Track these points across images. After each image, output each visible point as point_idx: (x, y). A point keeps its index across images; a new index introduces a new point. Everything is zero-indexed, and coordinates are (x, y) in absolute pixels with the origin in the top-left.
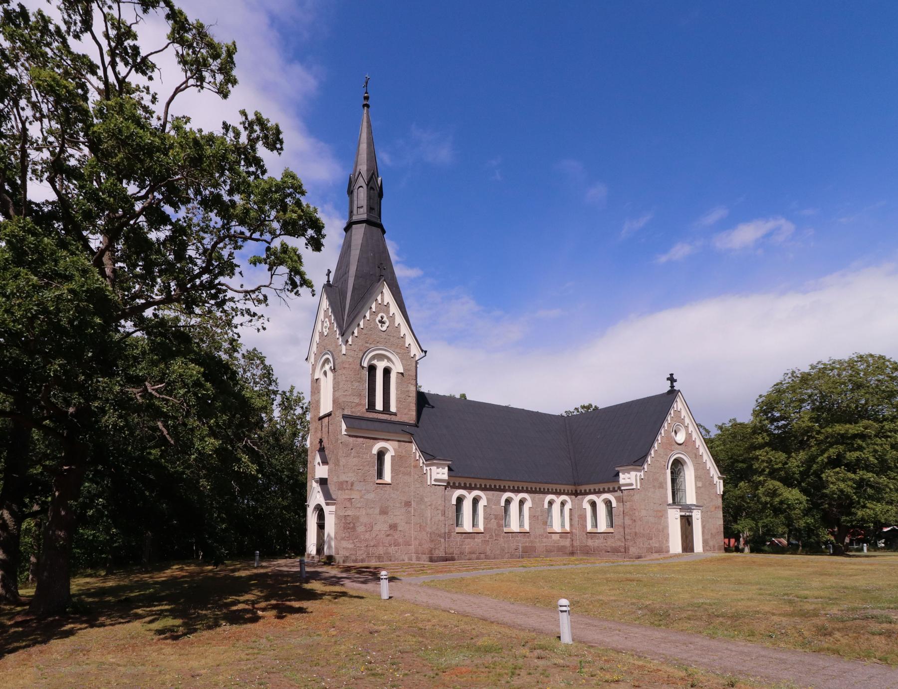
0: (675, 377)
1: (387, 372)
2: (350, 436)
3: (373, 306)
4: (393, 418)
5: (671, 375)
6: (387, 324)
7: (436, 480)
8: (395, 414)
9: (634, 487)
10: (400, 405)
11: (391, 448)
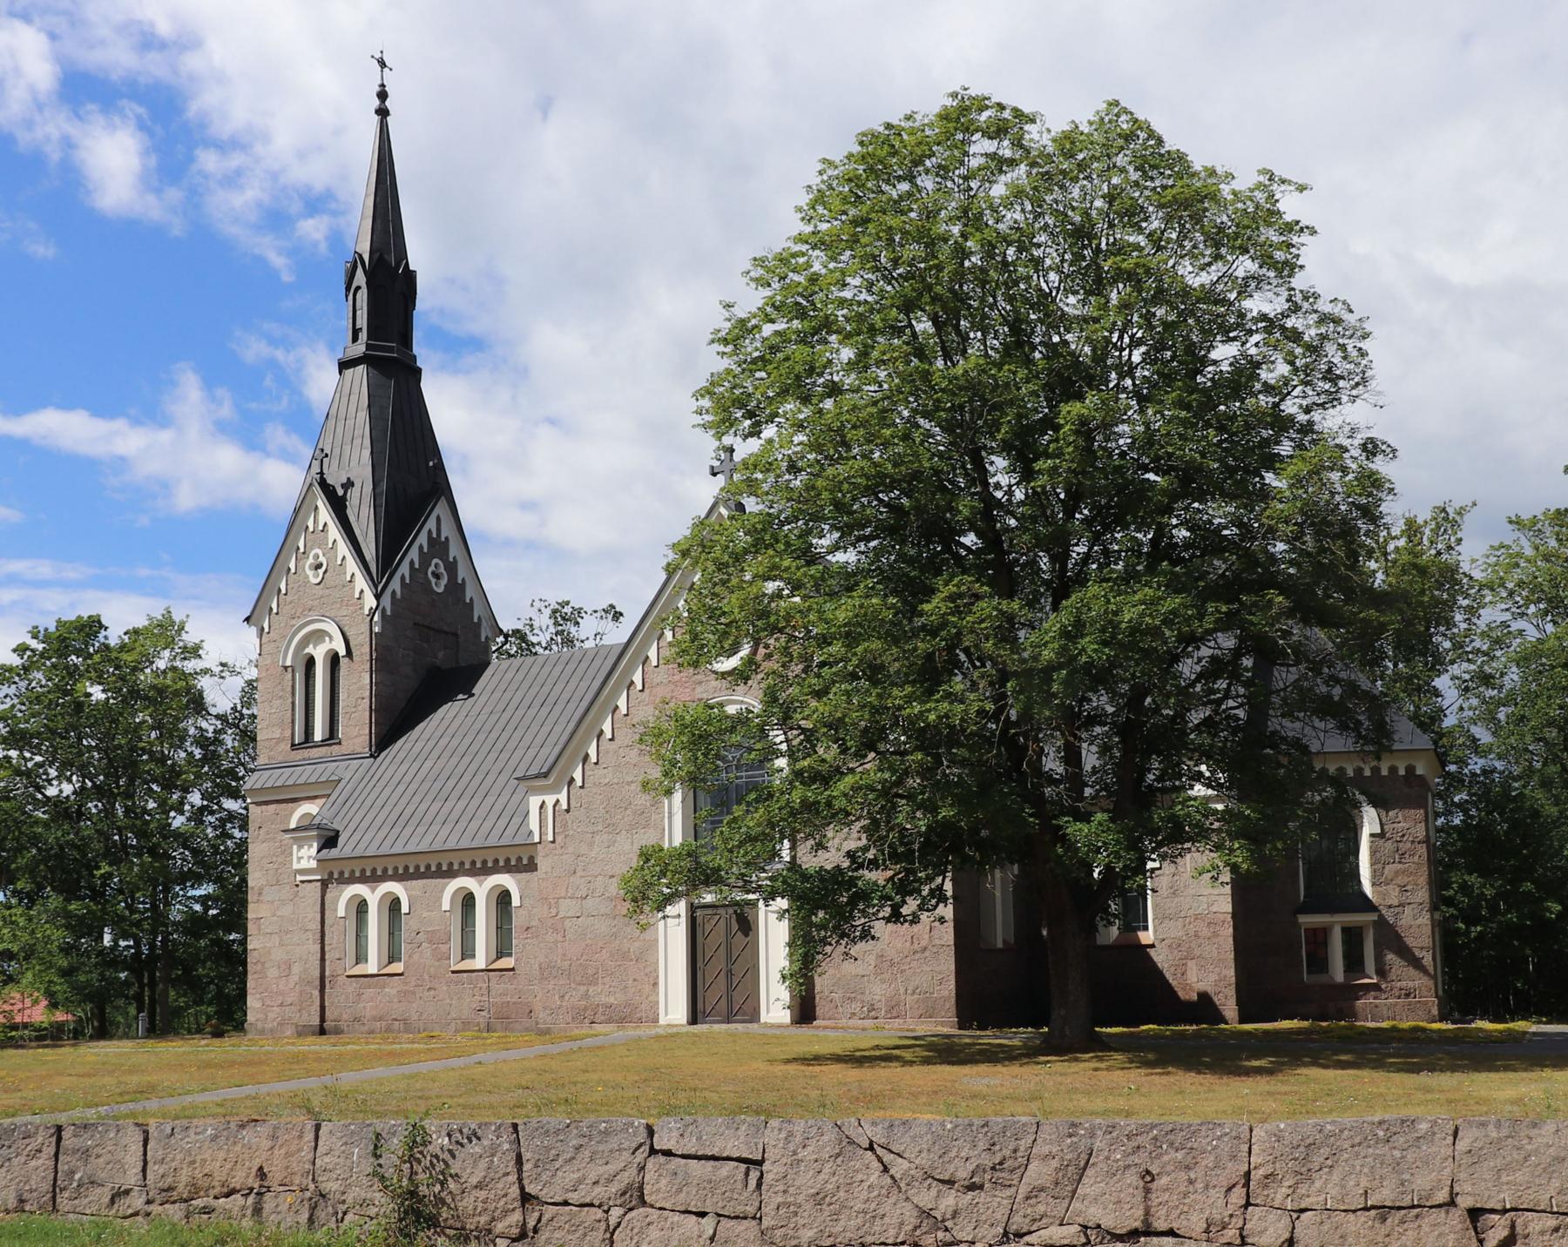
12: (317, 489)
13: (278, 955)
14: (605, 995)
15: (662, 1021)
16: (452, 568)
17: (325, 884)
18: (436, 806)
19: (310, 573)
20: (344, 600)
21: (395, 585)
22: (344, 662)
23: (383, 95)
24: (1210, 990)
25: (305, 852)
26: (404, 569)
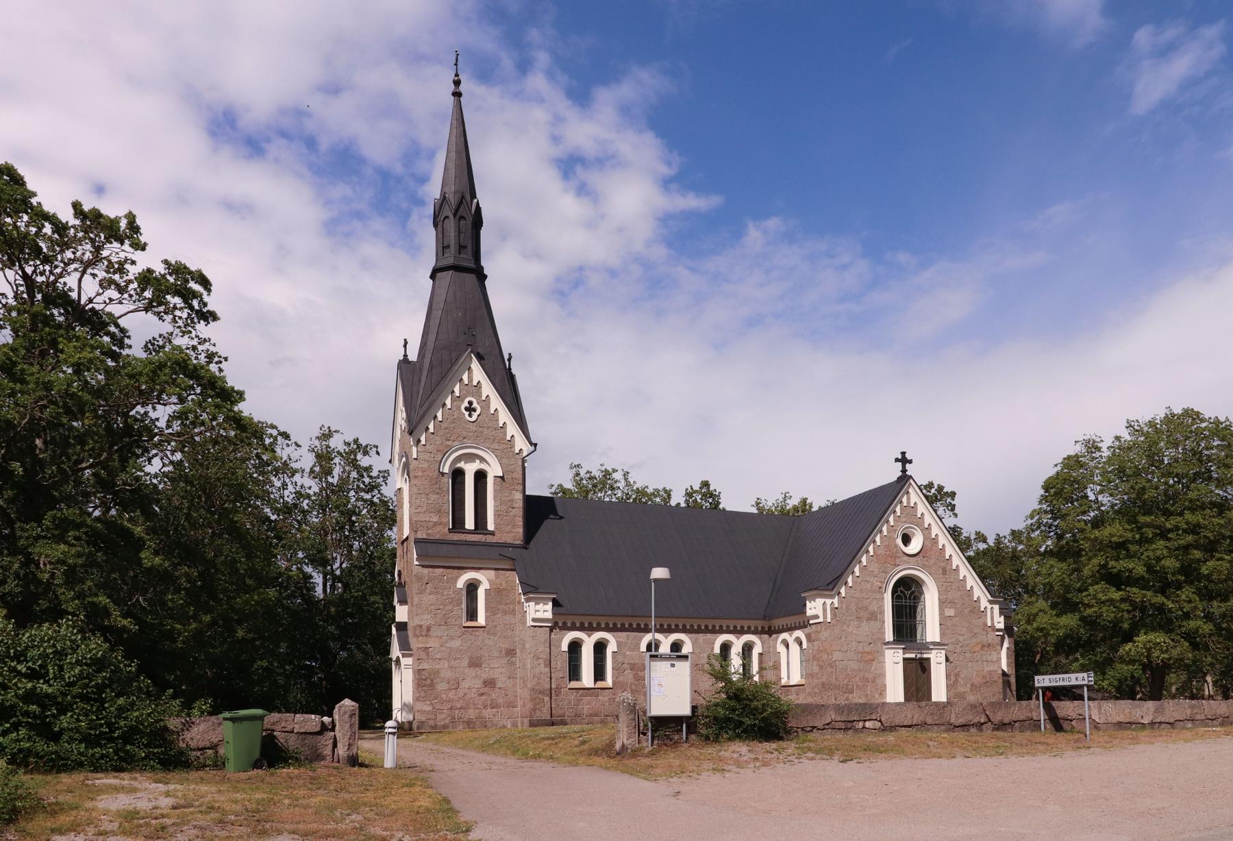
0: (908, 456)
1: (480, 476)
2: (423, 566)
3: (457, 389)
4: (490, 539)
5: (903, 453)
6: (478, 411)
7: (534, 620)
8: (492, 533)
9: (821, 620)
10: (501, 517)
11: (484, 579)
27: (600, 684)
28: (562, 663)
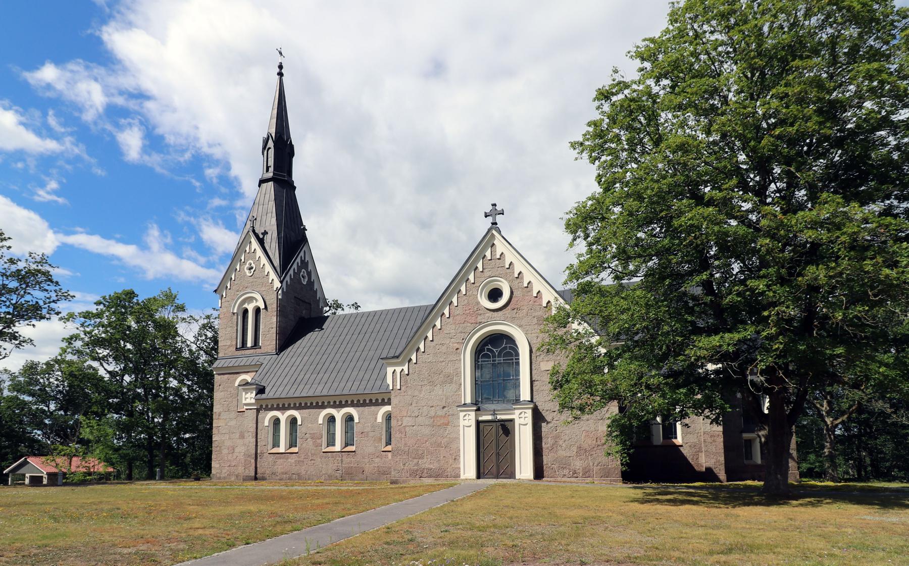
0: (489, 208)
12: (251, 234)
13: (228, 443)
14: (426, 463)
15: (462, 477)
16: (309, 274)
17: (258, 411)
18: (314, 376)
19: (247, 271)
20: (265, 284)
21: (288, 278)
22: (262, 312)
23: (281, 67)
24: (712, 466)
25: (248, 395)
26: (291, 272)
27: (330, 449)
28: (266, 436)
